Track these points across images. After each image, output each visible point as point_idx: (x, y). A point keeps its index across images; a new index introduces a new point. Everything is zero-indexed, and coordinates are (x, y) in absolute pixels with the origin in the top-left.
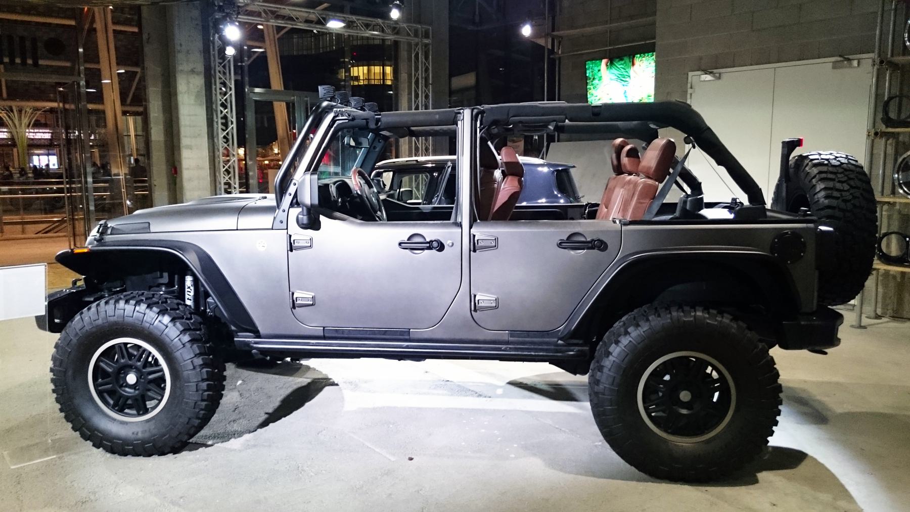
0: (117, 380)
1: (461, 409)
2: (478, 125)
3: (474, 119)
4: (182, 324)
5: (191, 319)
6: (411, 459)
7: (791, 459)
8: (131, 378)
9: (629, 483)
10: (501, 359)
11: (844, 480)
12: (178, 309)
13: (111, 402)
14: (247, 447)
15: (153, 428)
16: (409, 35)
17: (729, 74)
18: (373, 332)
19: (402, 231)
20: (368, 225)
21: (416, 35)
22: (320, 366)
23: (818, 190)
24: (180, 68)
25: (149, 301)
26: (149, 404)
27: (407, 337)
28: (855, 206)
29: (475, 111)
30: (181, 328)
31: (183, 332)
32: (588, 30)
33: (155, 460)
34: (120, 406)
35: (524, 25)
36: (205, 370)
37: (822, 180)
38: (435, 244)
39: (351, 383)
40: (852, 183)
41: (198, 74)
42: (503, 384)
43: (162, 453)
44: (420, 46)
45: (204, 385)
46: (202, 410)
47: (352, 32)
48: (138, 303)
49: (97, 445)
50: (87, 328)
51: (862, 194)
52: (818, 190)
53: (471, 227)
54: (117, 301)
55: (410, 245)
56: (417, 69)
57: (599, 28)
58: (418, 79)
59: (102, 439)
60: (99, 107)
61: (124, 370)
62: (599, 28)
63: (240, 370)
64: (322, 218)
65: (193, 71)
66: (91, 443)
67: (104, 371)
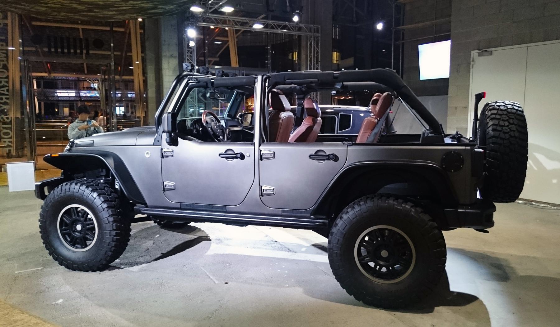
0: (72, 228)
1: (274, 258)
2: (267, 85)
3: (264, 81)
4: (103, 198)
5: (111, 195)
6: (227, 283)
7: (465, 299)
8: (79, 227)
9: (348, 306)
10: (228, 222)
11: (492, 315)
12: (104, 189)
13: (69, 239)
14: (141, 270)
15: (81, 256)
16: (306, 32)
17: (498, 52)
18: (206, 207)
19: (222, 148)
20: (204, 143)
21: (311, 31)
22: (205, 227)
23: (489, 125)
24: (164, 54)
25: (89, 184)
26: (88, 242)
27: (225, 210)
28: (510, 135)
29: (265, 77)
30: (103, 200)
31: (104, 202)
32: (420, 25)
33: (82, 273)
34: (74, 242)
35: (379, 23)
36: (115, 224)
37: (492, 119)
38: (239, 155)
39: (219, 240)
40: (511, 121)
41: (175, 57)
42: (309, 245)
43: (94, 271)
44: (313, 38)
45: (114, 233)
46: (113, 247)
47: (269, 31)
48: (81, 185)
49: (61, 264)
50: (56, 198)
51: (517, 129)
52: (489, 125)
53: (259, 146)
54: (71, 184)
55: (225, 155)
56: (311, 53)
57: (428, 23)
58: (311, 58)
59: (63, 260)
60: (131, 77)
61: (75, 222)
62: (428, 23)
63: (161, 229)
64: (179, 139)
65: (172, 56)
66: (58, 263)
67: (66, 223)
